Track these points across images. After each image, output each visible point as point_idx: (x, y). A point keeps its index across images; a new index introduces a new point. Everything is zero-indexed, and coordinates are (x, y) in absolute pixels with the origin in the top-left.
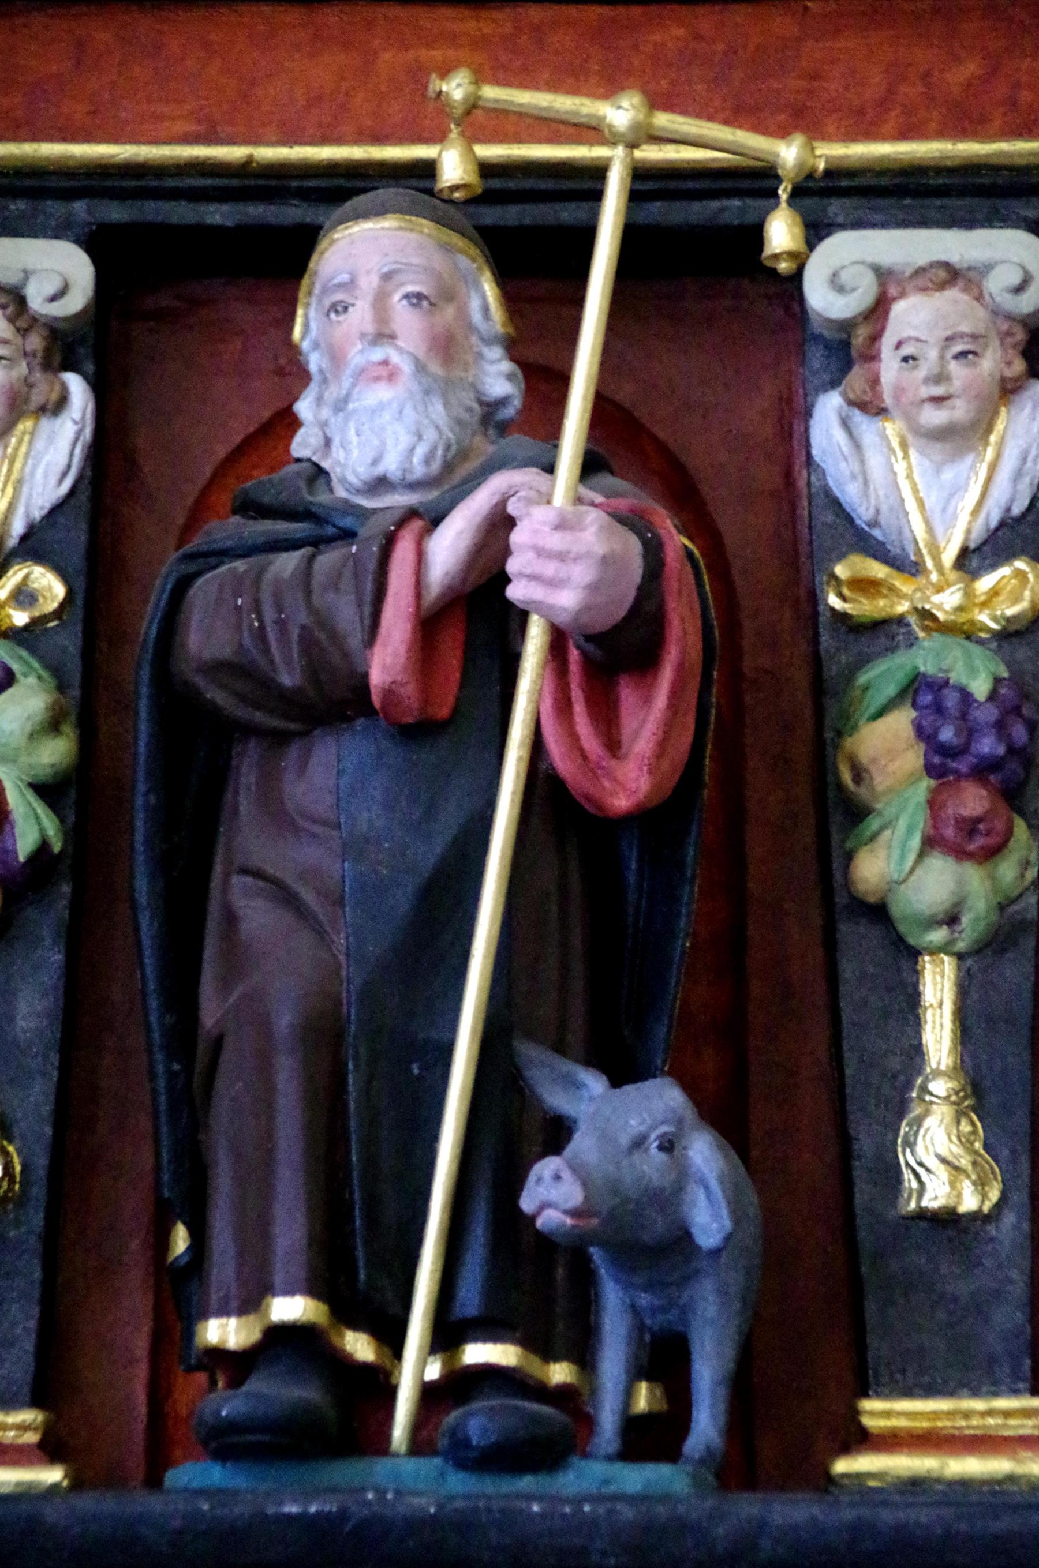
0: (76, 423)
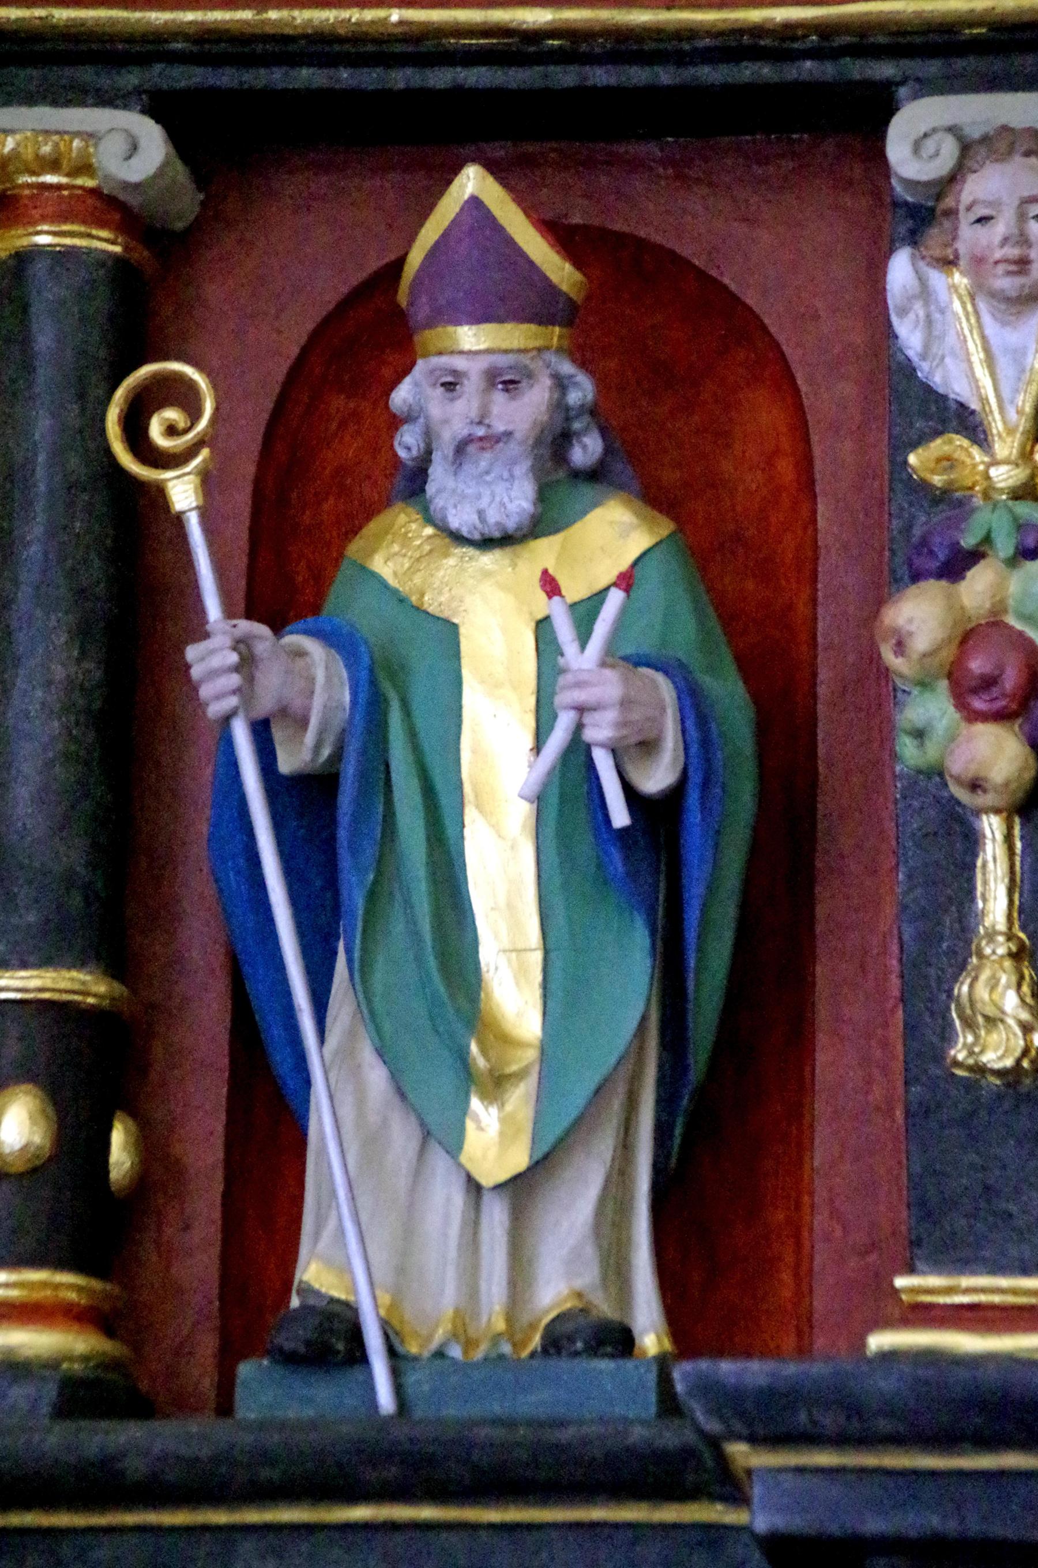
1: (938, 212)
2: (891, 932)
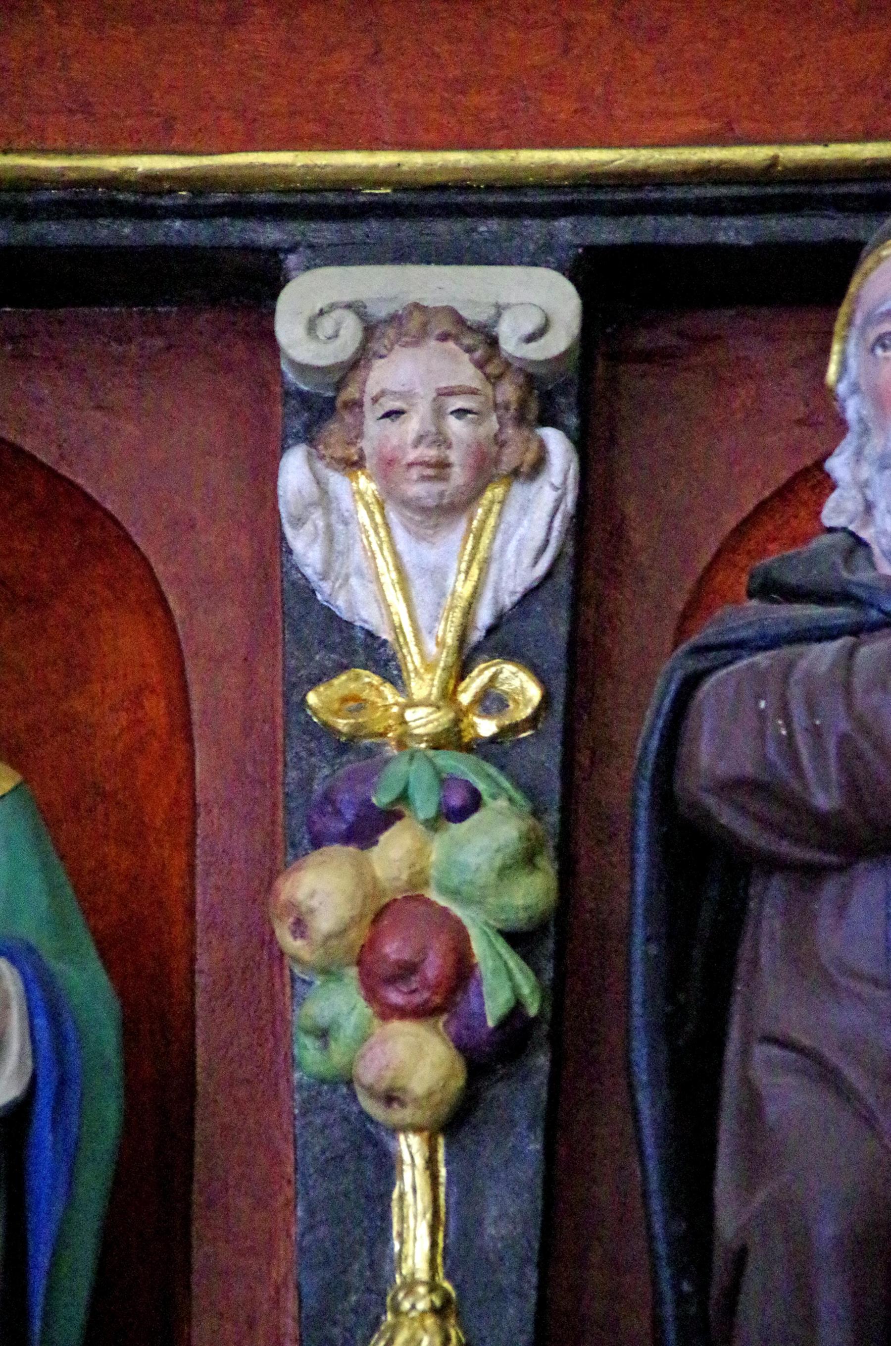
0: (556, 489)
1: (339, 403)
2: (285, 1284)
